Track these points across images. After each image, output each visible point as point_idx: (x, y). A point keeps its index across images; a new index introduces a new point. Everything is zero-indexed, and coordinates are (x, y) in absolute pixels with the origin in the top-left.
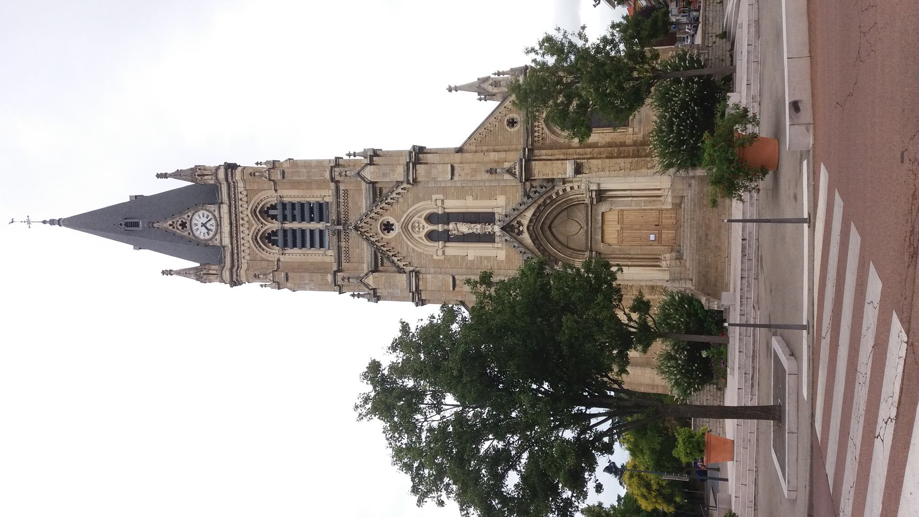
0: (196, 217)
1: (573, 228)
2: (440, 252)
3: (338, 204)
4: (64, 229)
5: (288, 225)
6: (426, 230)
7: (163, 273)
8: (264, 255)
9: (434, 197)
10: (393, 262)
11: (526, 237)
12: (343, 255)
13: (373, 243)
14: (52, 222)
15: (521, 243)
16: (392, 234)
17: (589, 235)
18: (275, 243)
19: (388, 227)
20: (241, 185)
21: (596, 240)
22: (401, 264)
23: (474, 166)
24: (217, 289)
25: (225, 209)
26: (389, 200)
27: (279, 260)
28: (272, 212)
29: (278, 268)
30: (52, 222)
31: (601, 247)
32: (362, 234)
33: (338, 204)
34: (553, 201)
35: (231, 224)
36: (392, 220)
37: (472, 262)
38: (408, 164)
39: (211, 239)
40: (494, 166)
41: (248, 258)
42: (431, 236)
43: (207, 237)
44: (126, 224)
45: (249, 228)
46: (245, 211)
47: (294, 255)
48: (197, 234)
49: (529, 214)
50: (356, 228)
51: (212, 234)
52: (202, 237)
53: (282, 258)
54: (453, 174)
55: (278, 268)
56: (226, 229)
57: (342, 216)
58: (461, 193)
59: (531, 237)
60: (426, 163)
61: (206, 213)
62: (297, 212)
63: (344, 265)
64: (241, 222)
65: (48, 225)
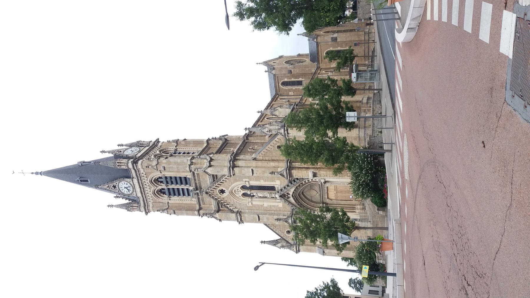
0: (120, 184)
1: (313, 193)
2: (250, 204)
3: (195, 180)
4: (43, 177)
5: (171, 187)
6: (242, 193)
7: (108, 206)
8: (160, 200)
9: (244, 180)
10: (227, 207)
11: (292, 200)
12: (201, 202)
13: (216, 199)
14: (37, 173)
15: (290, 202)
16: (225, 195)
17: (322, 196)
18: (164, 193)
19: (222, 192)
20: (142, 171)
21: (325, 198)
22: (231, 208)
23: (263, 169)
24: (138, 215)
25: (135, 181)
26: (221, 181)
27: (168, 203)
28: (160, 180)
29: (169, 206)
30: (37, 173)
31: (328, 201)
32: (210, 195)
33: (195, 180)
34: (303, 185)
35: (140, 188)
36: (224, 189)
37: (266, 207)
38: (230, 167)
39: (131, 194)
40: (274, 170)
41: (152, 201)
42: (244, 195)
43: (128, 193)
44: (81, 181)
45: (150, 190)
46: (146, 181)
47: (175, 200)
48: (123, 191)
49: (292, 190)
50: (207, 193)
51: (131, 192)
52: (126, 193)
53: (170, 202)
54: (253, 173)
55: (169, 206)
56: (138, 189)
57: (198, 185)
58: (258, 179)
59: (294, 199)
60: (238, 167)
61: (126, 183)
62: (173, 180)
63: (202, 206)
64: (145, 186)
65: (34, 175)
